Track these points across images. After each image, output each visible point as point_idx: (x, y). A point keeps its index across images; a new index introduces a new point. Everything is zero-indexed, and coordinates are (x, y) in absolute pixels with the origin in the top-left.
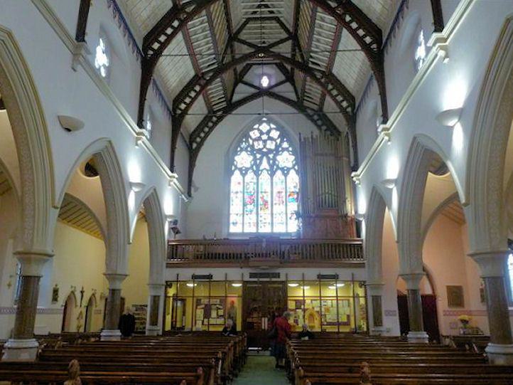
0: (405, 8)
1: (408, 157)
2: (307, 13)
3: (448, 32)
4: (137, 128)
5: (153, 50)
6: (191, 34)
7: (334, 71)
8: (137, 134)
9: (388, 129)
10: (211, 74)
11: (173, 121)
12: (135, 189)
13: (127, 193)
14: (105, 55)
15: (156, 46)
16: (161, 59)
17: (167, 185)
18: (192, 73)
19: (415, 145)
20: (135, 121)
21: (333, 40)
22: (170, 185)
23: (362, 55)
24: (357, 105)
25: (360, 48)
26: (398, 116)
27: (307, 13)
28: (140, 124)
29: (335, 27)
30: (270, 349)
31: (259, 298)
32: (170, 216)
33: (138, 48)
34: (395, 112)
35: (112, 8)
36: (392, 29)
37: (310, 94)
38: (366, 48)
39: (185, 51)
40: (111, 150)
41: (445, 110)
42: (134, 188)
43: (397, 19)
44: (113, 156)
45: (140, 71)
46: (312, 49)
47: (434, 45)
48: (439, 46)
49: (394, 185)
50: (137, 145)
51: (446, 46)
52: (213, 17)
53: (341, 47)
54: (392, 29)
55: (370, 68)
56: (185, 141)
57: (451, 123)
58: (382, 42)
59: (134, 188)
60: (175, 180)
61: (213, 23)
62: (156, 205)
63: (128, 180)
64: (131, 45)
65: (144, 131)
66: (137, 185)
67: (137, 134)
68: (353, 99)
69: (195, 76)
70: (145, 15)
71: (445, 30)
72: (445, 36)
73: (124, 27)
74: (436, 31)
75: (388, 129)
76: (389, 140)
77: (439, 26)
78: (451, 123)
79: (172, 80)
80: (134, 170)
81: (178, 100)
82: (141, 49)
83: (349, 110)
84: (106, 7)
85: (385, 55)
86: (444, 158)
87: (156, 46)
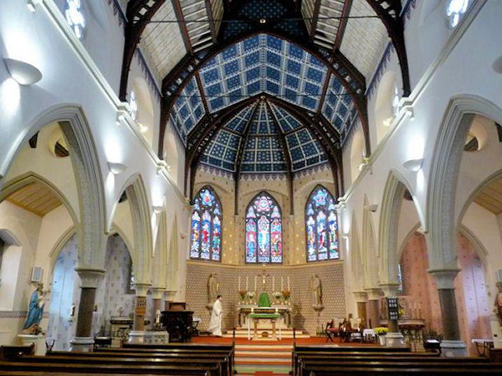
0: (411, 7)
1: (437, 143)
2: (310, 8)
3: (413, 98)
4: (158, 159)
5: (139, 15)
6: (190, 36)
7: (342, 49)
8: (159, 164)
9: (411, 103)
10: (216, 115)
11: (186, 152)
12: (114, 171)
13: (104, 177)
14: (80, 13)
15: (143, 11)
16: (149, 27)
17: (155, 171)
18: (184, 52)
19: (391, 177)
20: (115, 93)
21: (342, 12)
22: (158, 174)
23: (379, 22)
24: (367, 87)
25: (376, 14)
26: (419, 93)
27: (310, 8)
28: (123, 96)
29: (343, 4)
30: (250, 28)
31: (250, 294)
32: (158, 208)
33: (120, 11)
34: (423, 78)
35: (117, 15)
36: (374, 80)
37: (322, 35)
38: (382, 14)
39: (173, 16)
40: (140, 181)
41: (408, 160)
42: (112, 170)
43: (377, 73)
44: (83, 123)
45: (124, 38)
46: (317, 30)
47: (403, 105)
48: (407, 108)
49: (419, 167)
50: (118, 120)
51: (412, 108)
52: (212, 9)
53: (352, 13)
54: (374, 80)
55: (387, 35)
56: (156, 89)
57: (415, 169)
58: (401, 8)
59: (112, 170)
60: (163, 168)
61: (211, 6)
62: (141, 192)
63: (104, 157)
64: (140, 65)
65: (163, 162)
66: (117, 166)
67: (118, 108)
68: (363, 79)
69: (187, 54)
70: (164, 63)
71: (410, 96)
72: (411, 100)
73: (114, 5)
74: (404, 96)
75: (411, 103)
76: (412, 116)
77: (407, 91)
78: (415, 169)
79: (162, 56)
80: (112, 147)
81: (168, 81)
82: (124, 13)
83: (391, 12)
84: (118, 24)
85: (368, 100)
86: (411, 194)
87: (143, 11)
